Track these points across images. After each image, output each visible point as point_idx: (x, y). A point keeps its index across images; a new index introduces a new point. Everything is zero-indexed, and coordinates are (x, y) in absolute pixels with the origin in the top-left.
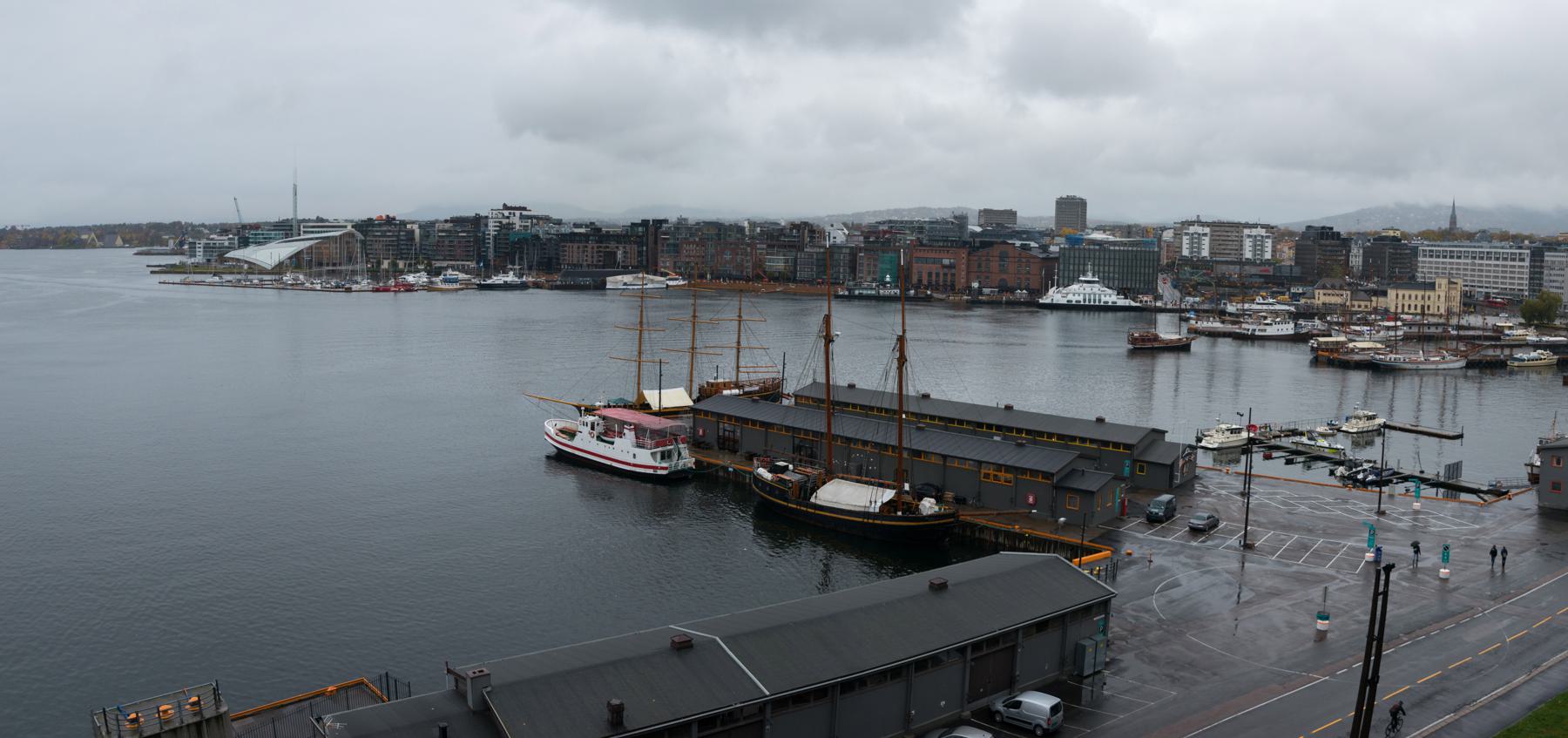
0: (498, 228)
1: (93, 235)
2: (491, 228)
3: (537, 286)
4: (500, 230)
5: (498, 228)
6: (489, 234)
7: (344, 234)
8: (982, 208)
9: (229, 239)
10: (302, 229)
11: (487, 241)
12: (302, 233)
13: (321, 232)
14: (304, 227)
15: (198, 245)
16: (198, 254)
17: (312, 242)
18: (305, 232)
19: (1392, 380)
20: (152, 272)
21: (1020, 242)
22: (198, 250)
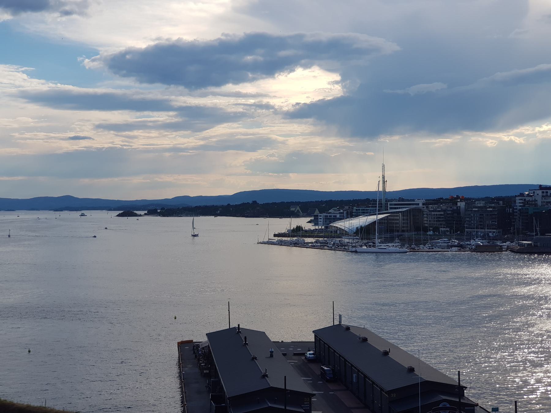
0: (522, 204)
1: (298, 208)
2: (518, 204)
3: (377, 386)
4: (523, 206)
5: (522, 204)
6: (516, 209)
7: (410, 210)
8: (180, 341)
9: (340, 213)
10: (389, 206)
11: (515, 214)
12: (389, 208)
13: (399, 208)
14: (390, 205)
15: (319, 217)
16: (319, 223)
17: (408, 209)
18: (391, 208)
19: (92, 128)
20: (413, 200)
21: (440, 406)
22: (319, 220)
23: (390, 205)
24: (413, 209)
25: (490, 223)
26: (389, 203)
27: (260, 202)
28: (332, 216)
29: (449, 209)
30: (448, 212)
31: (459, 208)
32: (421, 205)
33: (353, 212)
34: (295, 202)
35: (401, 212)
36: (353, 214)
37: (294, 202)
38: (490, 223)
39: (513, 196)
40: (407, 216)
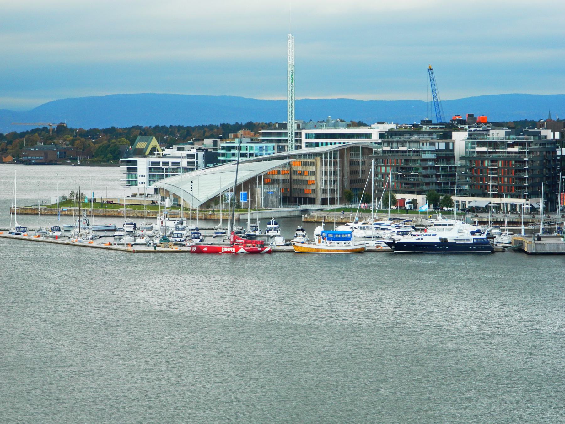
10: (304, 140)
12: (303, 145)
14: (307, 136)
16: (140, 180)
23: (307, 136)
24: (353, 149)
25: (42, 158)
26: (304, 132)
27: (74, 123)
28: (170, 164)
29: (427, 147)
30: (425, 156)
31: (451, 147)
32: (375, 138)
33: (219, 155)
34: (171, 126)
35: (320, 154)
36: (219, 158)
37: (169, 126)
38: (42, 158)
39: (206, 125)
40: (335, 164)
